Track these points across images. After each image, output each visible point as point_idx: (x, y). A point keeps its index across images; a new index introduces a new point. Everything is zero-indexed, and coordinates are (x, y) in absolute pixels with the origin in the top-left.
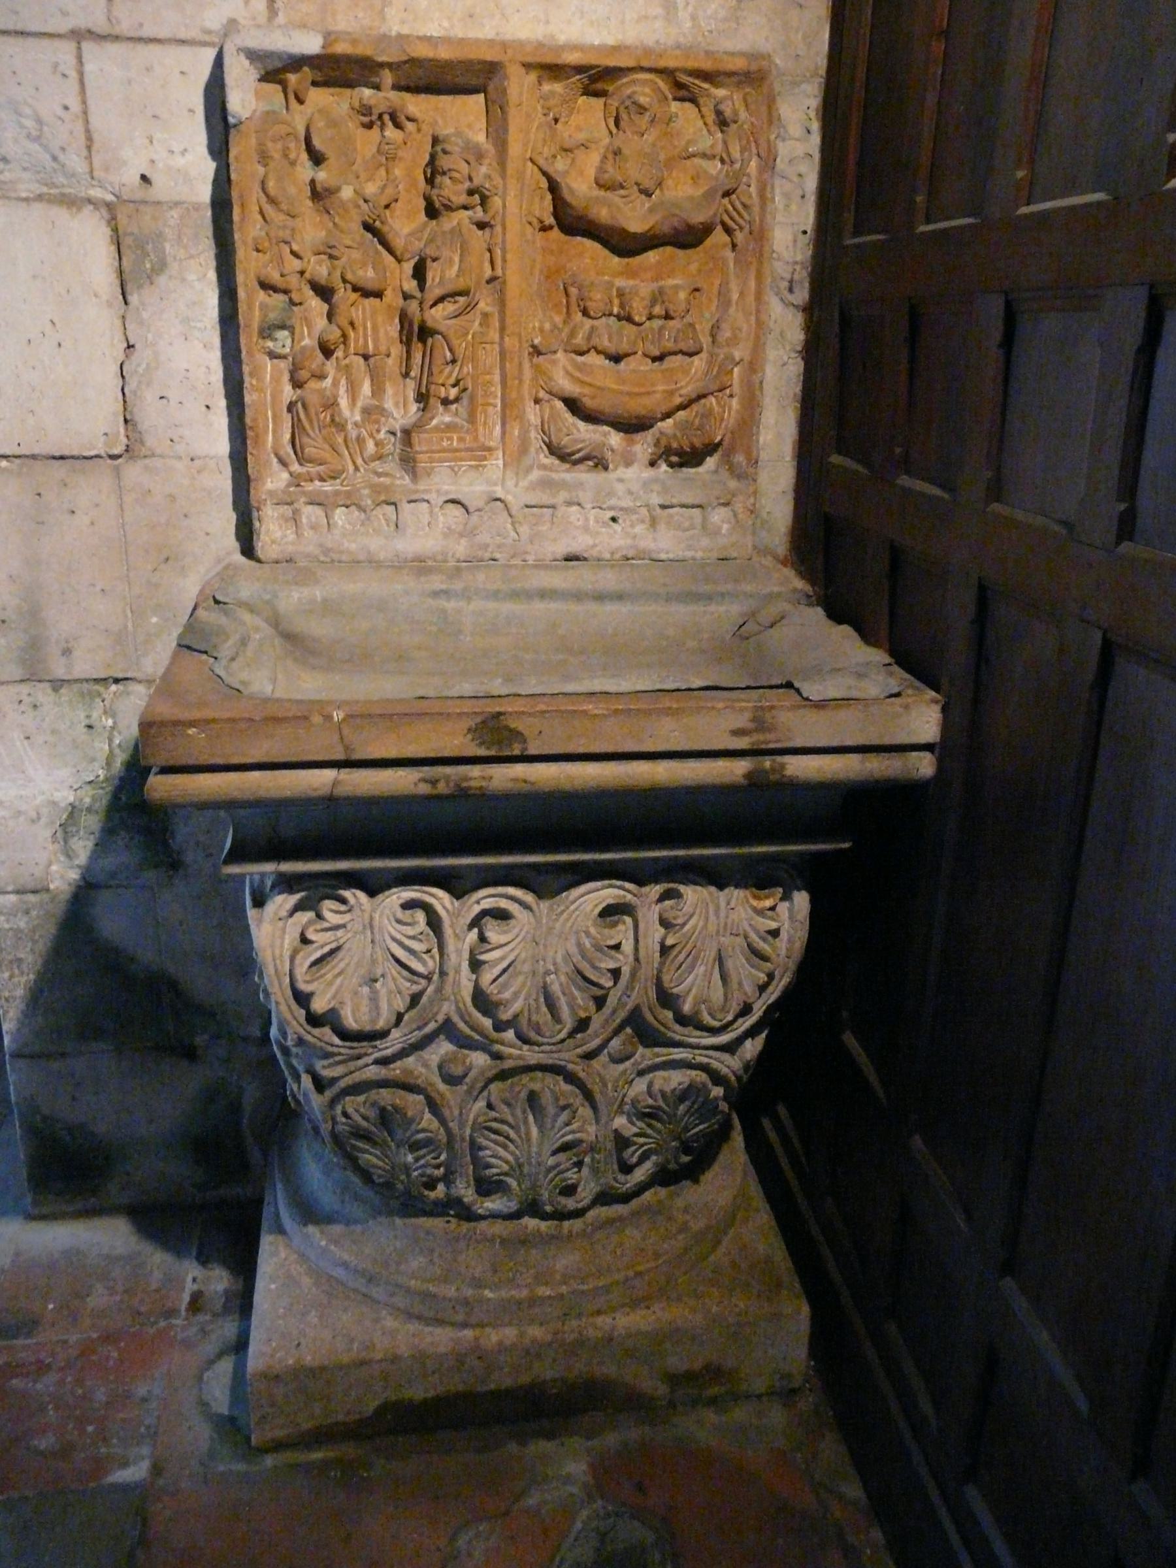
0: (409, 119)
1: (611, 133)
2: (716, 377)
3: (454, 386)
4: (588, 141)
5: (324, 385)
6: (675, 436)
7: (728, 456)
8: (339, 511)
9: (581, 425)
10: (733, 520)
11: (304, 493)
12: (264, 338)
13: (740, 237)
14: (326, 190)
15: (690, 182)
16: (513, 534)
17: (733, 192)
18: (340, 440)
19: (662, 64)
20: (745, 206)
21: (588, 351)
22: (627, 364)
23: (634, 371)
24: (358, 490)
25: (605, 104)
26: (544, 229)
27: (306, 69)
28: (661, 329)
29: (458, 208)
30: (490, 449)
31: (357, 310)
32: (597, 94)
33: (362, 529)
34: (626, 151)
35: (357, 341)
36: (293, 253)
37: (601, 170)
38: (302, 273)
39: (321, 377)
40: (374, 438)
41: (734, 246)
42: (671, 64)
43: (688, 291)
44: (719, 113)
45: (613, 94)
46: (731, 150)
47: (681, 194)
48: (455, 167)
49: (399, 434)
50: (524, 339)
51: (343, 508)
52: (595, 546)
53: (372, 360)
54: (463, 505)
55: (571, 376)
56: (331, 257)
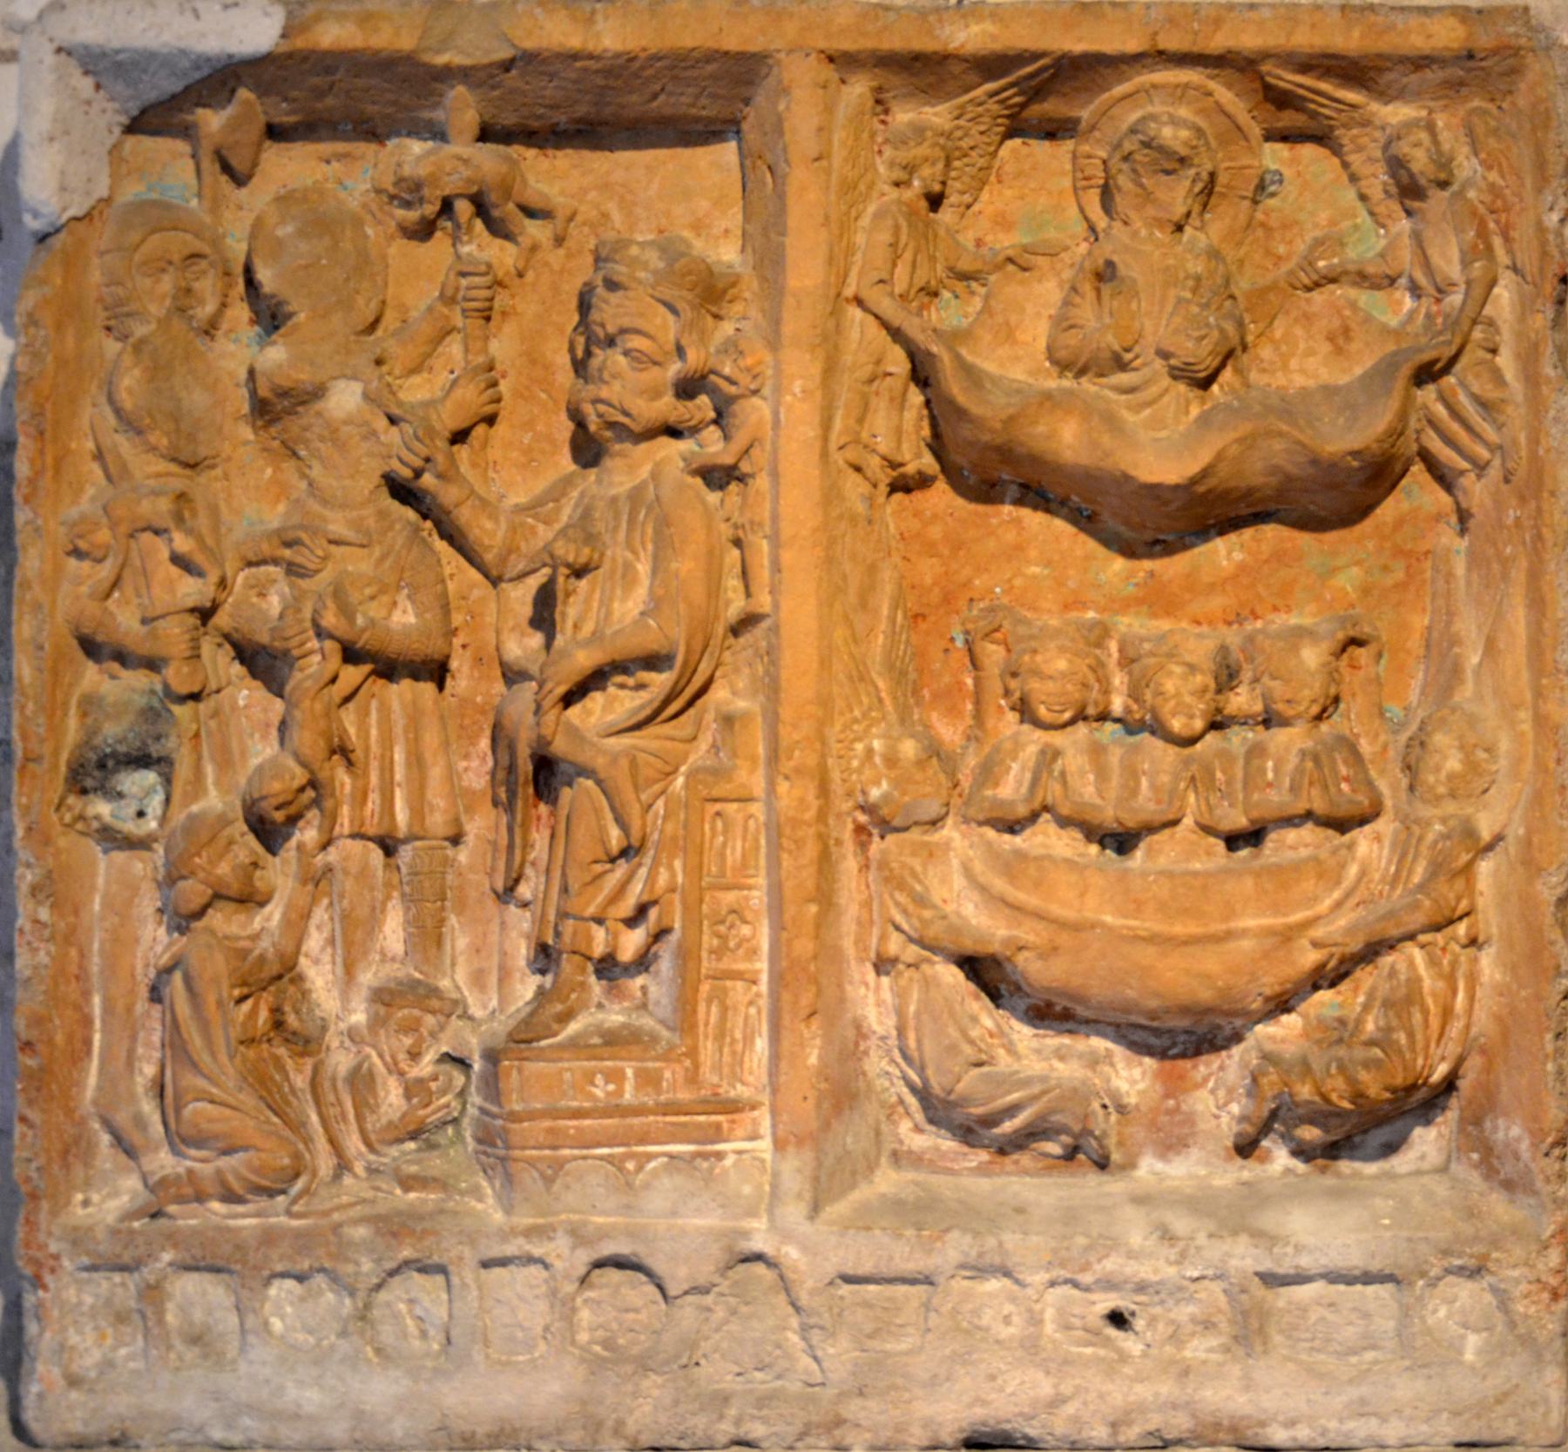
0: (530, 213)
1: (1092, 229)
2: (1421, 887)
3: (632, 922)
4: (1026, 249)
5: (257, 923)
6: (1305, 1067)
7: (1478, 1122)
8: (281, 1290)
9: (1022, 1033)
10: (1499, 1320)
11: (173, 1239)
12: (84, 792)
13: (1477, 491)
14: (284, 394)
15: (1326, 347)
16: (806, 1361)
17: (1447, 369)
18: (300, 1081)
19: (1218, 42)
20: (1484, 404)
21: (1033, 817)
22: (1150, 853)
23: (1169, 875)
24: (336, 1228)
25: (1075, 157)
26: (904, 485)
27: (243, 94)
28: (1256, 752)
29: (650, 434)
30: (732, 1107)
31: (364, 713)
32: (1053, 131)
33: (344, 1346)
34: (1129, 268)
35: (361, 797)
36: (178, 560)
37: (1063, 323)
38: (205, 614)
39: (250, 899)
40: (402, 1074)
41: (1463, 516)
42: (1249, 41)
43: (1326, 647)
44: (1396, 165)
45: (1093, 128)
46: (1436, 259)
47: (1299, 381)
48: (639, 323)
49: (477, 1067)
50: (837, 787)
51: (290, 1284)
52: (1057, 1402)
53: (405, 854)
54: (649, 1273)
55: (983, 889)
56: (293, 570)
